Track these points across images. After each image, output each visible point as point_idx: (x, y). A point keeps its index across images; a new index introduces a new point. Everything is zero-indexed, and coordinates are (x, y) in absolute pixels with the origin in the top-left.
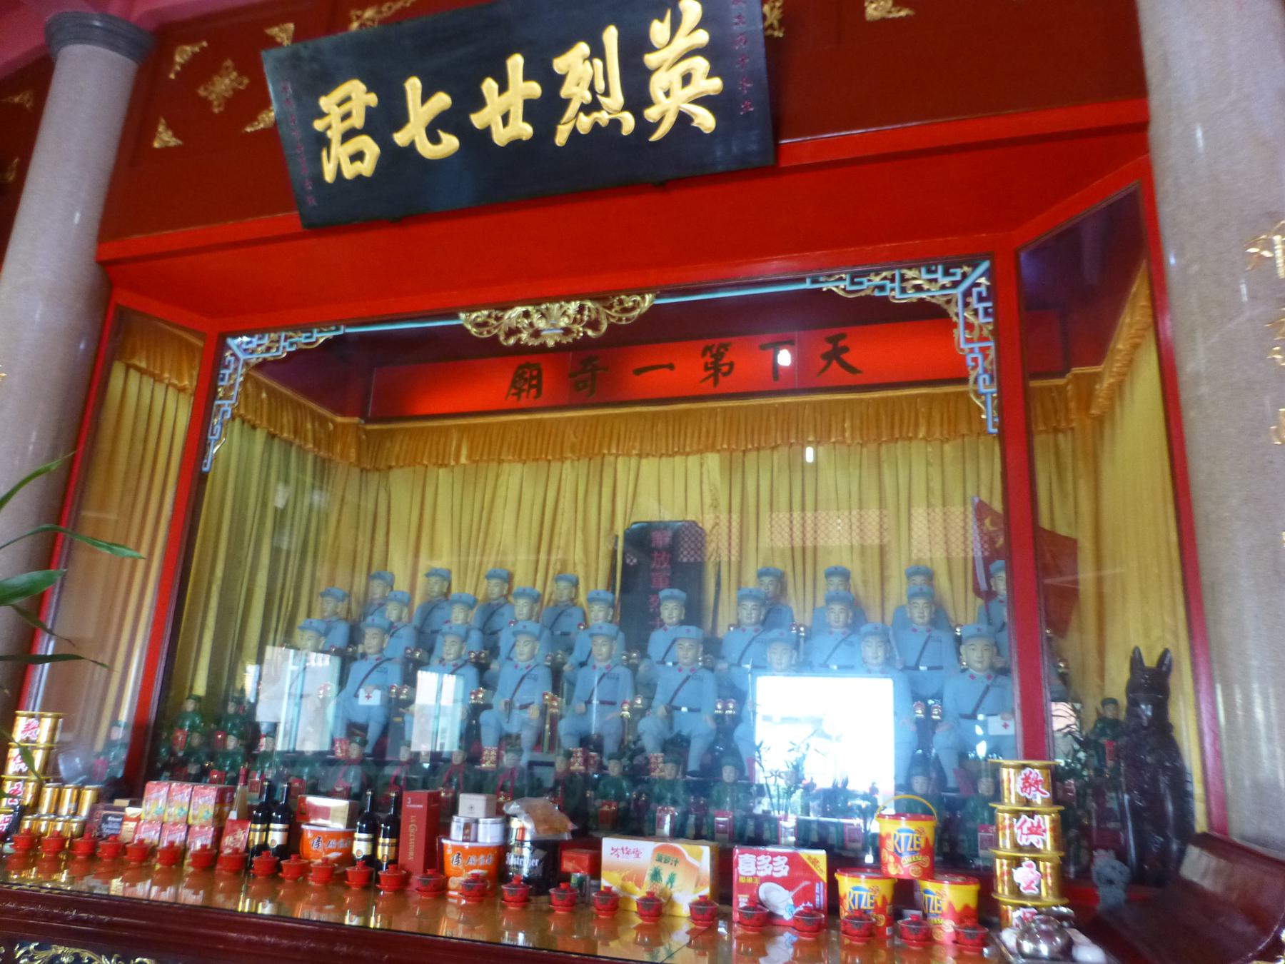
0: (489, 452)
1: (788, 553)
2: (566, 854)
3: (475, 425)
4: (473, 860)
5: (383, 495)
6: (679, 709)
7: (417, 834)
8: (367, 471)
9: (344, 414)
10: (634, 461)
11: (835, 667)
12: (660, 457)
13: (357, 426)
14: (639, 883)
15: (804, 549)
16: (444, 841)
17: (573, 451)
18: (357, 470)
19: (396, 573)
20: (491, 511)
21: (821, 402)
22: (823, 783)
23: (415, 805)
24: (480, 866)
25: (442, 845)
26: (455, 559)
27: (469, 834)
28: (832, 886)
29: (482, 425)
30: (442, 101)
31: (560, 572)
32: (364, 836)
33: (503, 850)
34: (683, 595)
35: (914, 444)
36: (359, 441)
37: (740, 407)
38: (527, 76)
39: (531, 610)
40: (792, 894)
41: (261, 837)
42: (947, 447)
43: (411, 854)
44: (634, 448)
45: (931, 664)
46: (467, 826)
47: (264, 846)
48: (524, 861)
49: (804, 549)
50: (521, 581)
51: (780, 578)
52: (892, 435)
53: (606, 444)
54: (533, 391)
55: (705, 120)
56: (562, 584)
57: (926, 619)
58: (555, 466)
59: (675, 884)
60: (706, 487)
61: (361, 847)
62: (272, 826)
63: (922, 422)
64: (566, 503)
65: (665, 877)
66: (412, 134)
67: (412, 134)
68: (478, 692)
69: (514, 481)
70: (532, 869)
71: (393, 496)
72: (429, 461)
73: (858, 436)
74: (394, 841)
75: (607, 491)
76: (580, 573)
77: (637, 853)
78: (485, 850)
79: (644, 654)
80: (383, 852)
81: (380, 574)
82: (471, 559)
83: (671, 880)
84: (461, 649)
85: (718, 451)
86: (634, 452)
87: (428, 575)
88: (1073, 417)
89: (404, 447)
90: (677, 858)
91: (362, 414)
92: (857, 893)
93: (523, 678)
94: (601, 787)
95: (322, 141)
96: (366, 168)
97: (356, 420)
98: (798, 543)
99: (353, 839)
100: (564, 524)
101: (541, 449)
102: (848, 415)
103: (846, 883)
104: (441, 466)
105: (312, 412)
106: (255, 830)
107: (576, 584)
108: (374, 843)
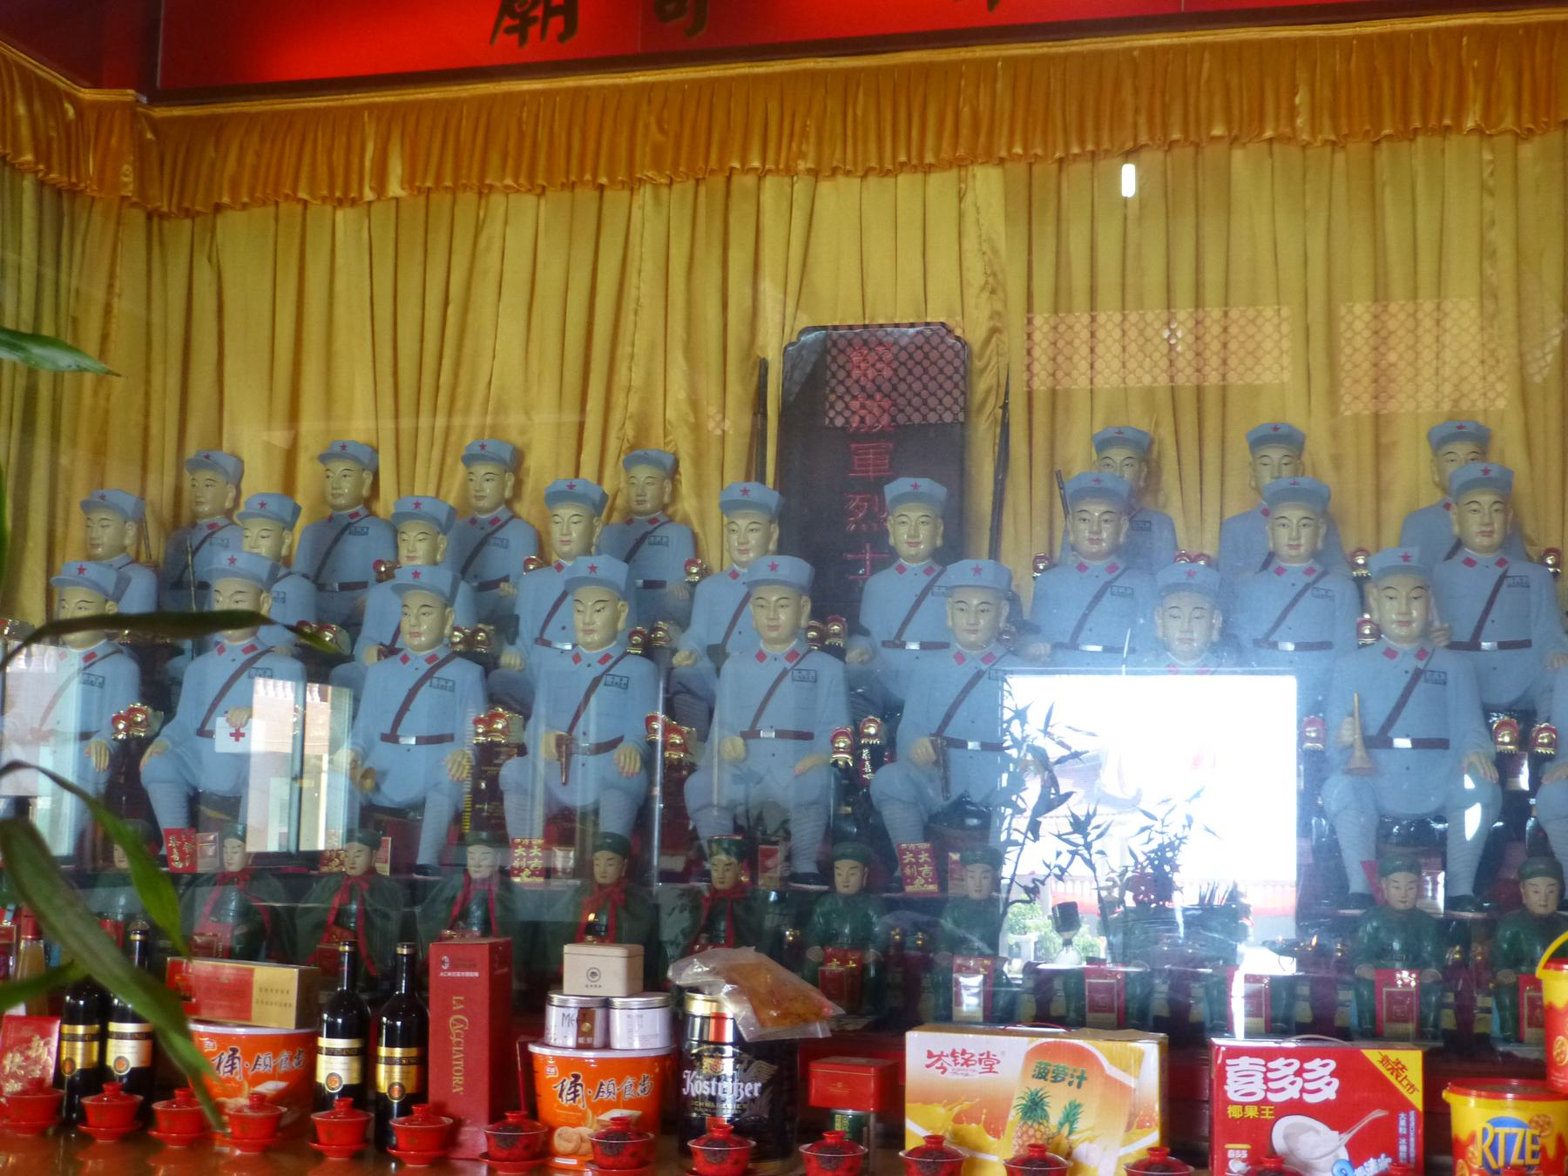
0: (460, 169)
1: (1163, 399)
2: (820, 1070)
3: (420, 106)
4: (609, 1088)
5: (204, 276)
6: (963, 745)
7: (468, 1036)
8: (162, 216)
9: (97, 84)
10: (801, 186)
11: (1290, 647)
12: (864, 176)
13: (130, 107)
14: (995, 1128)
15: (1199, 391)
16: (535, 1049)
17: (657, 165)
18: (138, 217)
19: (246, 456)
20: (465, 309)
21: (1241, 45)
23: (460, 974)
24: (622, 1101)
25: (529, 1058)
26: (387, 424)
27: (590, 1033)
28: (1436, 1118)
29: (436, 104)
31: (632, 448)
32: (340, 1043)
33: (675, 1062)
34: (940, 491)
35: (1454, 139)
36: (142, 150)
37: (1050, 58)
39: (590, 530)
40: (1346, 1137)
41: (87, 1053)
42: (1527, 151)
43: (458, 1079)
44: (802, 155)
45: (898, 651)
46: (585, 1015)
47: (98, 1074)
48: (725, 1087)
50: (545, 466)
51: (1145, 452)
52: (1406, 120)
53: (736, 146)
54: (556, 22)
56: (642, 473)
57: (1497, 537)
58: (616, 199)
59: (1079, 1126)
60: (970, 244)
61: (334, 1067)
62: (114, 1027)
63: (1474, 91)
64: (644, 285)
65: (1055, 1114)
68: (494, 717)
69: (520, 235)
70: (743, 1106)
71: (227, 276)
72: (312, 193)
73: (1327, 122)
74: (413, 1052)
75: (739, 258)
76: (684, 447)
77: (989, 1062)
78: (632, 1066)
79: (855, 628)
80: (390, 1076)
81: (215, 460)
82: (424, 422)
83: (1071, 1117)
84: (443, 621)
85: (1002, 161)
86: (802, 165)
87: (324, 458)
89: (250, 159)
90: (1082, 1069)
91: (143, 83)
92: (1502, 1131)
93: (596, 682)
94: (818, 919)
97: (130, 94)
98: (1186, 378)
99: (314, 1051)
100: (641, 332)
101: (572, 165)
102: (1302, 76)
103: (1472, 1114)
104: (340, 203)
105: (25, 75)
106: (74, 1038)
107: (673, 472)
108: (366, 1060)
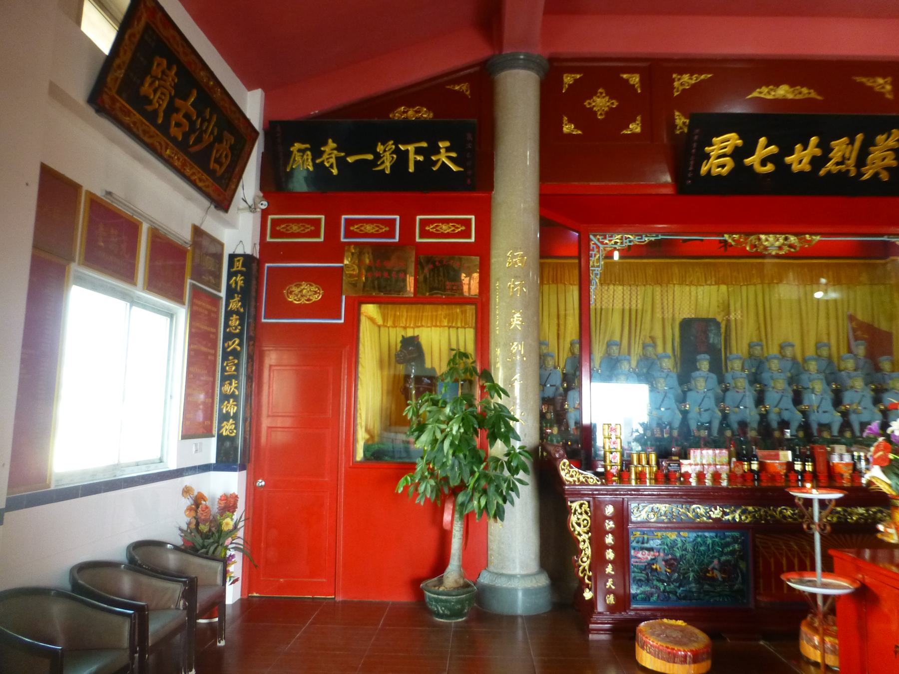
15: (630, 310)
22: (586, 421)
30: (773, 149)
38: (818, 146)
47: (751, 470)
49: (630, 310)
55: (885, 176)
66: (753, 160)
67: (753, 160)
88: (330, 153)
95: (707, 157)
96: (725, 171)
108: (804, 465)
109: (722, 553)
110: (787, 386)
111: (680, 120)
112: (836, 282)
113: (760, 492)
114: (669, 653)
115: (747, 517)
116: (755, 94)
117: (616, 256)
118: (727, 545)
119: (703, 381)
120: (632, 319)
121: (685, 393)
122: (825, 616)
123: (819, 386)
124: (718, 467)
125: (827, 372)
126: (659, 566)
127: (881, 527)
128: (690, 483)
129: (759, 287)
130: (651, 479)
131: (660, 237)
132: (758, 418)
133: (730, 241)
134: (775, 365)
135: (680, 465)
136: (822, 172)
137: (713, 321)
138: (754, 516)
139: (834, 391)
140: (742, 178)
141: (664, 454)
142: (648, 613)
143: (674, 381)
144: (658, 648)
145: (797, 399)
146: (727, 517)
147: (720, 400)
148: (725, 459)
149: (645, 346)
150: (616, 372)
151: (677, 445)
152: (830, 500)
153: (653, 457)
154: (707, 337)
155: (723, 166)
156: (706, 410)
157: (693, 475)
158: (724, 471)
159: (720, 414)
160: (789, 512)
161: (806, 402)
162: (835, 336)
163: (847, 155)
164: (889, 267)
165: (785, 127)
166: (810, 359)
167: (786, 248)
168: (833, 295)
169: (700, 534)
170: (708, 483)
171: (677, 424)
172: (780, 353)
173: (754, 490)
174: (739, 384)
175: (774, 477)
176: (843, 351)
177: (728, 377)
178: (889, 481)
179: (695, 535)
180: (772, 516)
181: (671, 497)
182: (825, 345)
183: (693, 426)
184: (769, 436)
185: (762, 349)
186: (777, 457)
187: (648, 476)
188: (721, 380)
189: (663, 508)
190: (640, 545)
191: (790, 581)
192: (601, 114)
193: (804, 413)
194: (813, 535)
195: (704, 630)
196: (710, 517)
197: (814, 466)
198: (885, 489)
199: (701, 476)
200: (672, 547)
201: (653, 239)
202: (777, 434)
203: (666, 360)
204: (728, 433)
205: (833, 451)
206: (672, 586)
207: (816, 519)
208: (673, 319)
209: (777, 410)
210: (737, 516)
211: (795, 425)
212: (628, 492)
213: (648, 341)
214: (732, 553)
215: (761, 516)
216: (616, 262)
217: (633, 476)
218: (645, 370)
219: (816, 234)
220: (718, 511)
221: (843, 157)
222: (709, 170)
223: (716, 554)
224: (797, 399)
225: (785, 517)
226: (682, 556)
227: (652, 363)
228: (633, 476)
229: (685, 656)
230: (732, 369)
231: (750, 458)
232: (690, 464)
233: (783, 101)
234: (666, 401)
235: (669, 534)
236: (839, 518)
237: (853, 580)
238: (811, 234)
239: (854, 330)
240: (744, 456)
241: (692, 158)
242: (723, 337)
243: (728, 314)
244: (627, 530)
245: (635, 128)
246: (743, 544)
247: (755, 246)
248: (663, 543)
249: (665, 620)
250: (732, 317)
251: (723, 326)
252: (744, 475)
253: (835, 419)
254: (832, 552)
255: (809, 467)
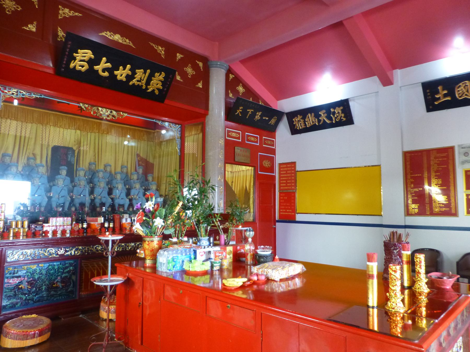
15: (21, 137)
30: (109, 65)
47: (83, 228)
55: (157, 92)
95: (75, 59)
96: (83, 69)
108: (109, 224)
109: (63, 273)
110: (106, 185)
111: (61, 33)
112: (133, 137)
113: (86, 239)
114: (24, 335)
115: (78, 252)
116: (103, 34)
117: (16, 102)
118: (67, 268)
119: (62, 180)
120: (21, 142)
121: (51, 187)
122: (111, 295)
123: (120, 186)
124: (65, 227)
125: (125, 180)
126: (24, 286)
127: (138, 251)
128: (48, 236)
129: (97, 134)
130: (23, 236)
131: (43, 97)
132: (90, 201)
133: (83, 107)
134: (101, 175)
135: (43, 227)
136: (131, 83)
137: (71, 149)
138: (82, 251)
139: (127, 189)
140: (90, 76)
141: (34, 221)
142: (13, 315)
143: (45, 180)
144: (17, 334)
145: (110, 192)
146: (67, 253)
147: (71, 191)
148: (70, 222)
149: (28, 159)
150: (6, 172)
151: (43, 216)
152: (117, 240)
153: (26, 223)
154: (67, 157)
155: (83, 66)
156: (62, 197)
157: (50, 232)
158: (68, 229)
159: (70, 199)
160: (100, 248)
161: (114, 194)
162: (129, 162)
163: (142, 78)
164: (156, 134)
165: (118, 57)
166: (118, 173)
167: (111, 117)
168: (133, 144)
169: (51, 264)
170: (59, 235)
171: (44, 204)
172: (104, 169)
173: (83, 238)
174: (82, 183)
175: (94, 231)
176: (133, 170)
177: (76, 179)
178: (142, 230)
179: (48, 265)
180: (91, 250)
181: (35, 245)
182: (125, 167)
183: (54, 205)
184: (94, 211)
185: (96, 166)
186: (97, 221)
187: (21, 234)
188: (72, 181)
189: (29, 251)
190: (11, 275)
191: (95, 281)
192: (8, 11)
193: (112, 199)
194: (108, 257)
195: (47, 317)
196: (57, 254)
197: (114, 225)
198: (141, 233)
199: (55, 232)
200: (33, 274)
201: (38, 97)
202: (98, 209)
203: (41, 168)
204: (73, 209)
205: (123, 217)
206: (31, 296)
207: (110, 250)
208: (48, 145)
209: (100, 197)
210: (73, 252)
211: (107, 205)
212: (7, 245)
213: (31, 156)
214: (68, 272)
215: (85, 251)
216: (15, 107)
217: (11, 235)
218: (27, 173)
219: (125, 113)
220: (63, 250)
221: (141, 78)
222: (75, 66)
223: (59, 274)
224: (110, 192)
225: (97, 250)
226: (38, 278)
227: (32, 169)
228: (11, 235)
229: (34, 334)
230: (79, 175)
231: (83, 221)
232: (49, 226)
233: (116, 43)
234: (39, 191)
235: (32, 266)
236: (123, 248)
237: (125, 277)
238: (123, 112)
239: (139, 161)
240: (80, 220)
241: (66, 57)
242: (76, 158)
243: (80, 147)
244: (4, 267)
245: (32, 28)
246: (75, 266)
247: (96, 113)
248: (27, 272)
249: (24, 316)
250: (82, 148)
251: (76, 152)
252: (78, 231)
253: (126, 202)
254: (116, 265)
255: (111, 225)
